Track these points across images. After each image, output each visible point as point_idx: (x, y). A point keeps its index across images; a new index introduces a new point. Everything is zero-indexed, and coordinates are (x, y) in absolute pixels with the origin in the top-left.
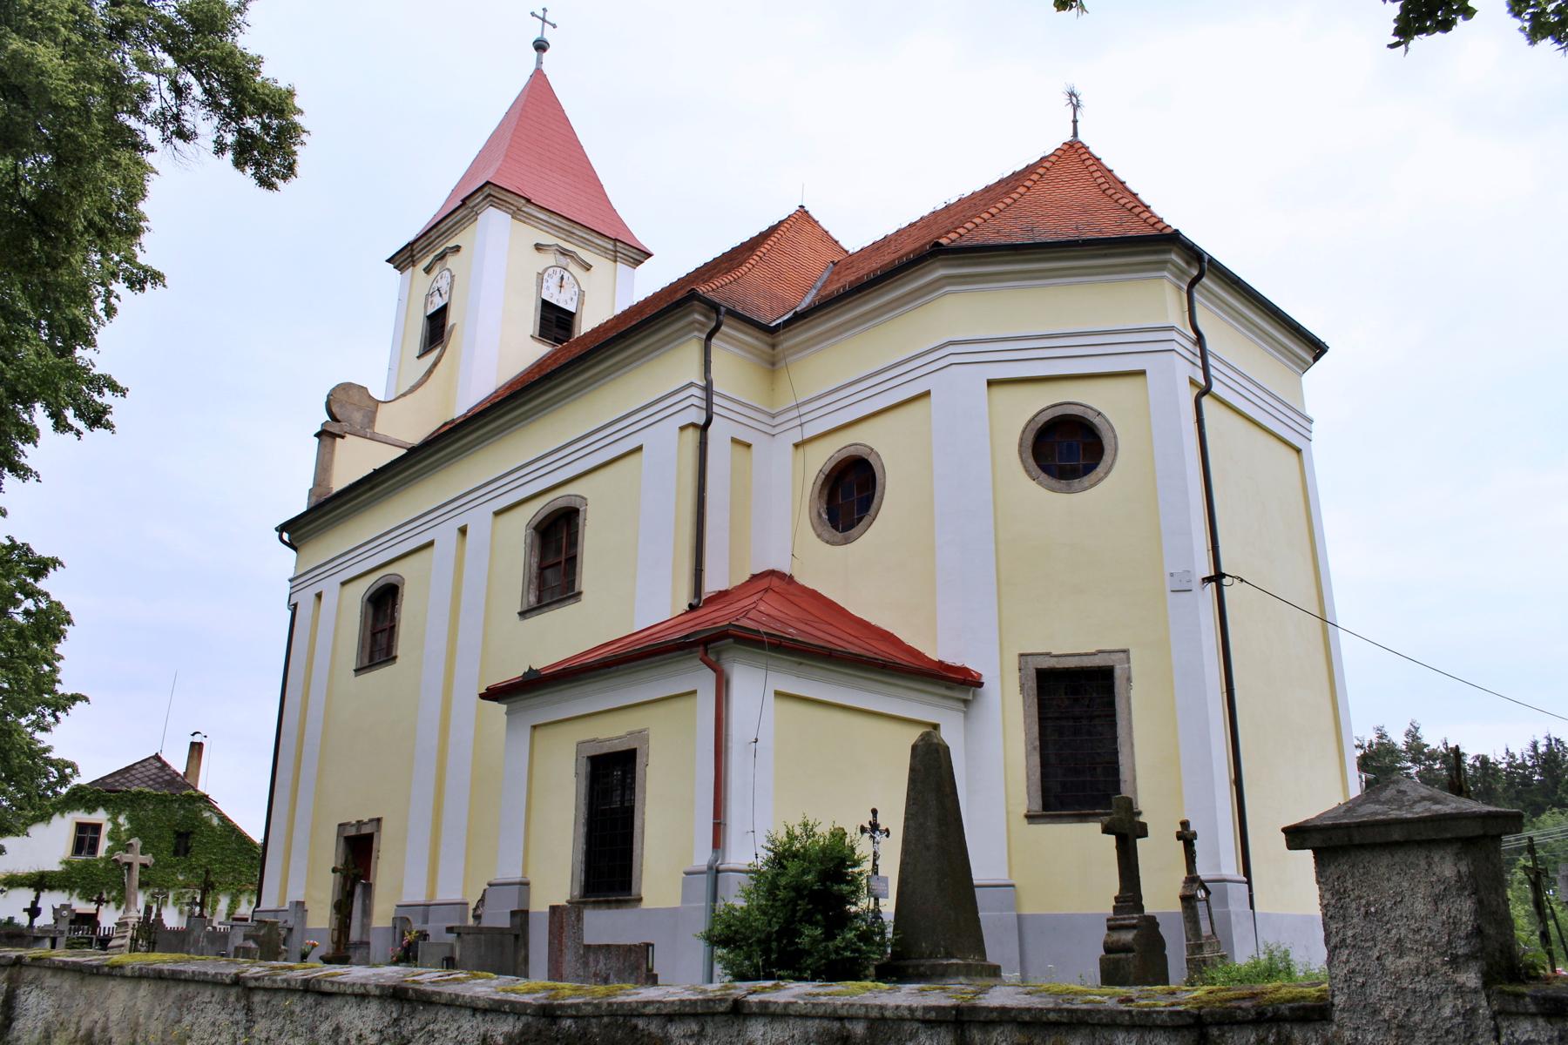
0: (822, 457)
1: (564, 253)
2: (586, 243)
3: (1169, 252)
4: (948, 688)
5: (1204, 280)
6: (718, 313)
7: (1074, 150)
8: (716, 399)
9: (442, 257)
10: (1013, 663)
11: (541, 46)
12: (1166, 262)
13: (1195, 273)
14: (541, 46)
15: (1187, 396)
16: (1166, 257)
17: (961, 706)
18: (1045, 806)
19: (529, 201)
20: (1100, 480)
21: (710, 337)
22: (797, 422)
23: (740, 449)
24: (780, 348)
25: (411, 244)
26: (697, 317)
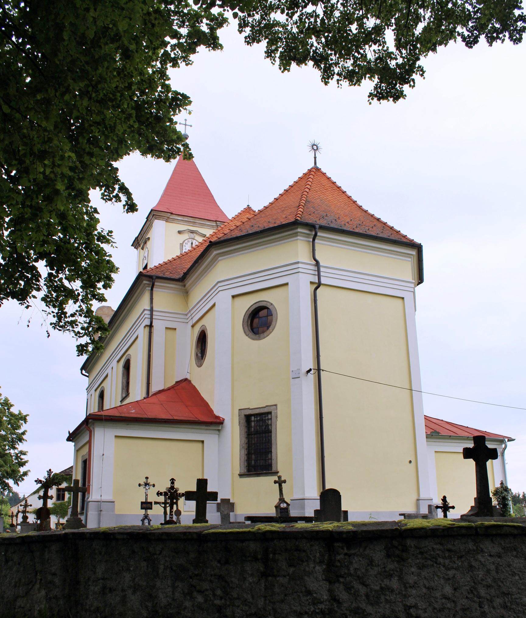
1: (192, 232)
2: (202, 225)
3: (297, 228)
4: (206, 426)
5: (156, 284)
6: (153, 279)
7: (315, 171)
8: (322, 269)
9: (145, 243)
10: (236, 412)
12: (297, 233)
13: (314, 233)
15: (307, 290)
16: (296, 231)
17: (217, 432)
18: (249, 470)
19: (172, 213)
20: (271, 333)
21: (314, 240)
22: (191, 318)
23: (170, 332)
24: (187, 286)
25: (137, 238)
26: (145, 282)
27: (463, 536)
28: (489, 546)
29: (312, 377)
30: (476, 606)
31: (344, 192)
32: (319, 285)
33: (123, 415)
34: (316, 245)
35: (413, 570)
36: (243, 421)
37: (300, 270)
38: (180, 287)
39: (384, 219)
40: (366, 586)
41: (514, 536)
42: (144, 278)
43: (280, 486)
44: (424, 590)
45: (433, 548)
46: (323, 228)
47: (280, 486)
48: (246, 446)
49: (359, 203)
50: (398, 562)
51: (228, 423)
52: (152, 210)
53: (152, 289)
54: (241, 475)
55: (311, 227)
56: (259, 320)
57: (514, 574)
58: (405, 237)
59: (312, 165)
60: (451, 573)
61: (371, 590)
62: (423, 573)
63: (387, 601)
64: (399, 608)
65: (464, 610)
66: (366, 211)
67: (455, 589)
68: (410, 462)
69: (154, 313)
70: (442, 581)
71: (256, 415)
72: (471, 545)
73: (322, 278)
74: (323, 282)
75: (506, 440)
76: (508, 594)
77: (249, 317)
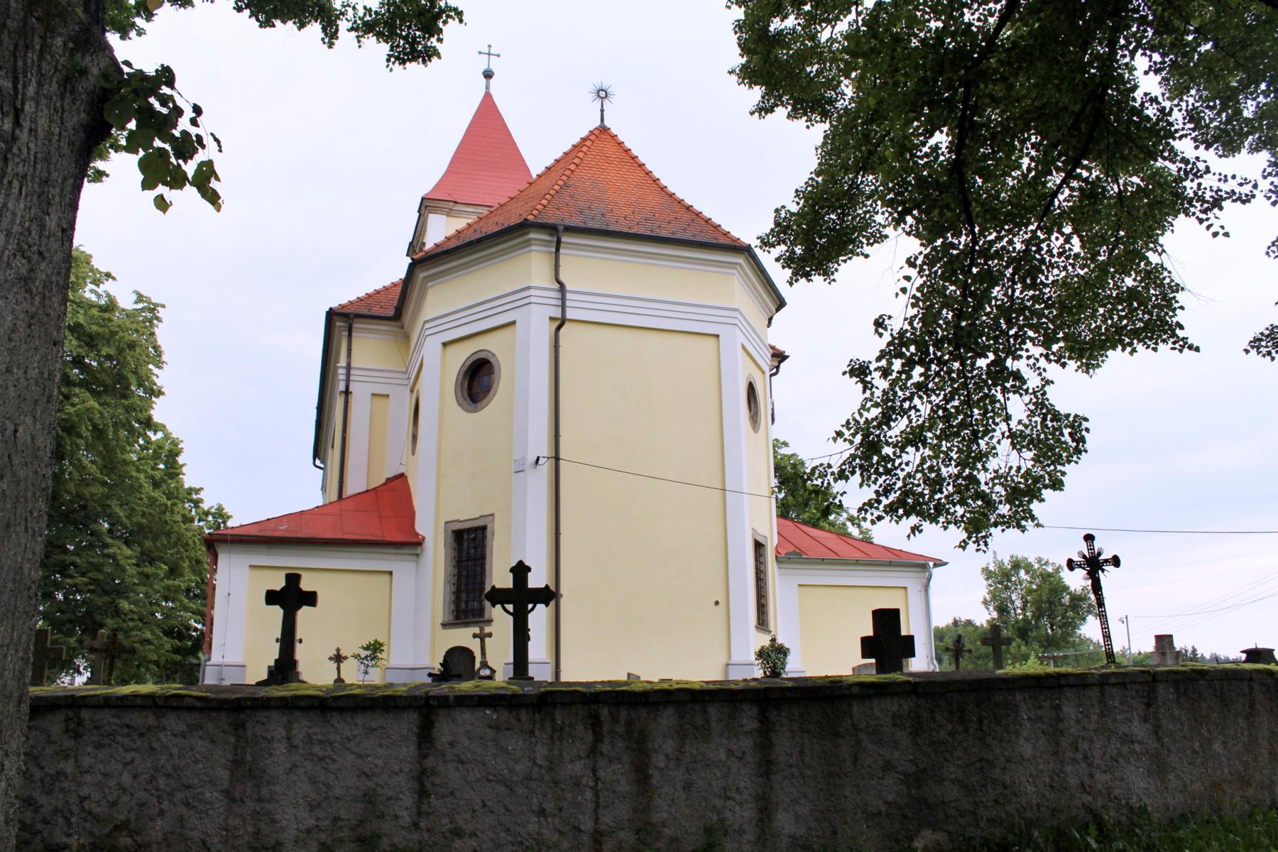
0: (461, 356)
3: (528, 233)
5: (355, 325)
8: (569, 296)
11: (488, 75)
12: (530, 240)
14: (488, 75)
15: (547, 330)
18: (457, 617)
21: (558, 250)
23: (379, 401)
25: (411, 244)
27: (143, 707)
28: (173, 722)
29: (545, 468)
30: (154, 801)
31: (641, 165)
32: (562, 322)
33: (262, 534)
34: (562, 258)
35: (89, 749)
36: (451, 539)
37: (532, 299)
38: (396, 329)
39: (697, 207)
40: (42, 768)
41: (201, 710)
42: (335, 317)
43: (483, 642)
44: (100, 777)
45: (110, 724)
46: (570, 230)
47: (483, 642)
48: (454, 580)
49: (664, 182)
50: (75, 739)
51: (429, 544)
52: (423, 199)
53: (350, 335)
54: (444, 625)
55: (552, 229)
56: (477, 380)
57: (197, 761)
58: (726, 234)
59: (598, 123)
60: (129, 756)
61: (47, 775)
62: (101, 755)
63: (62, 790)
64: (73, 799)
65: (142, 805)
66: (672, 195)
67: (135, 777)
68: (717, 603)
69: (353, 372)
70: (120, 766)
71: (469, 531)
72: (151, 720)
73: (568, 310)
74: (568, 316)
75: (931, 564)
76: (189, 787)
77: (465, 376)
